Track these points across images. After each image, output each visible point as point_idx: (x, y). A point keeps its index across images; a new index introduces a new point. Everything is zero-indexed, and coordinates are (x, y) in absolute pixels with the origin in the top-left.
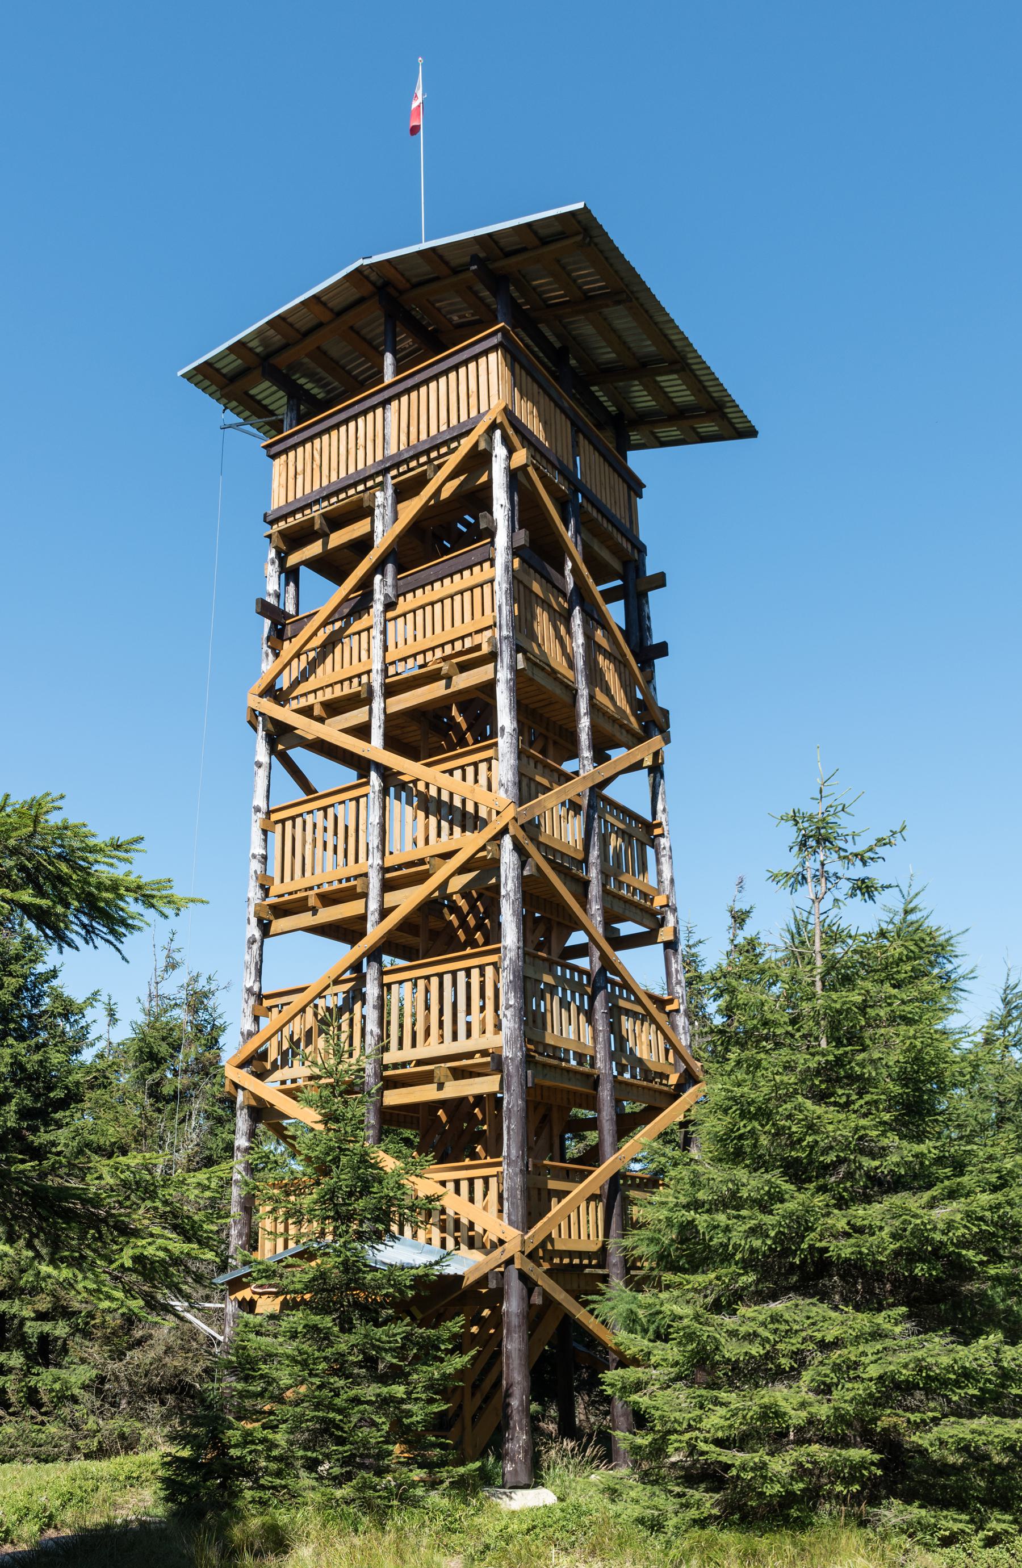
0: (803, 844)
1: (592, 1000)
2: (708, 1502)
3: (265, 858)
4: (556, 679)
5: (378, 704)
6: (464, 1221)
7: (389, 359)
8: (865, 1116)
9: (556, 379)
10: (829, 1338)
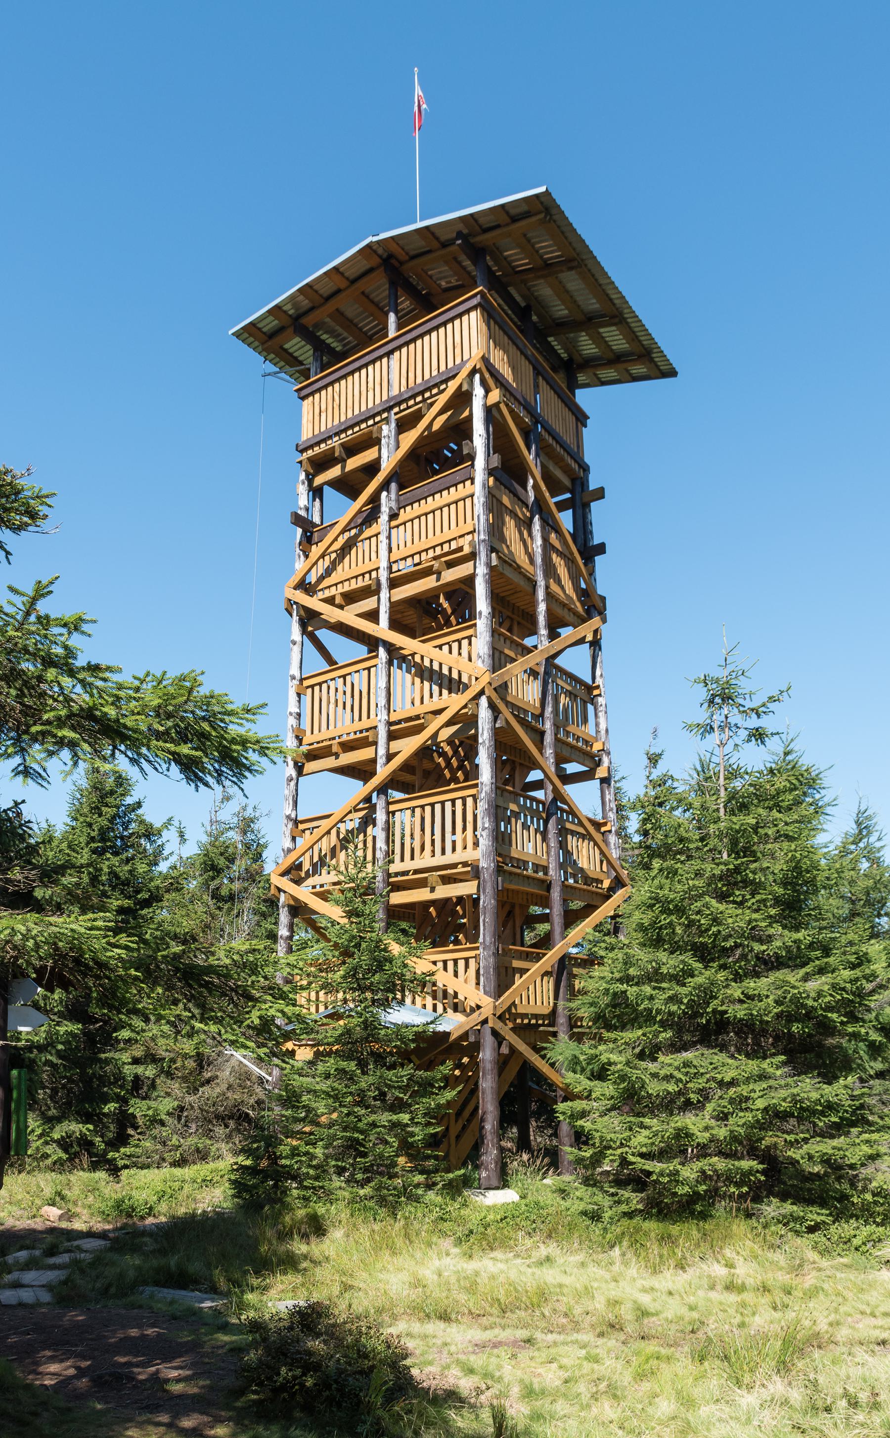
0: (711, 702)
1: (546, 823)
2: (634, 1199)
3: (299, 715)
4: (521, 573)
5: (384, 594)
6: (450, 991)
7: (392, 317)
8: (757, 911)
9: (522, 331)
10: (727, 1079)
